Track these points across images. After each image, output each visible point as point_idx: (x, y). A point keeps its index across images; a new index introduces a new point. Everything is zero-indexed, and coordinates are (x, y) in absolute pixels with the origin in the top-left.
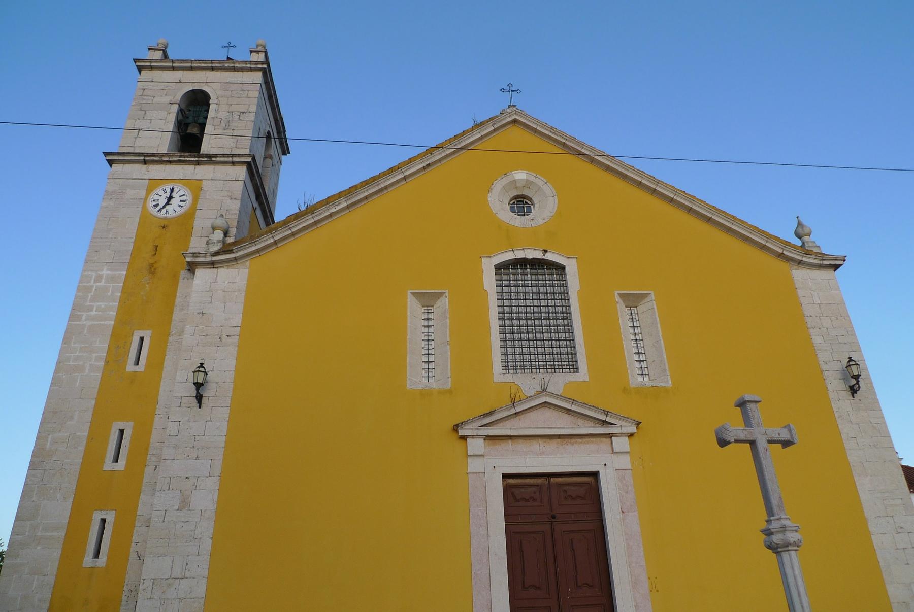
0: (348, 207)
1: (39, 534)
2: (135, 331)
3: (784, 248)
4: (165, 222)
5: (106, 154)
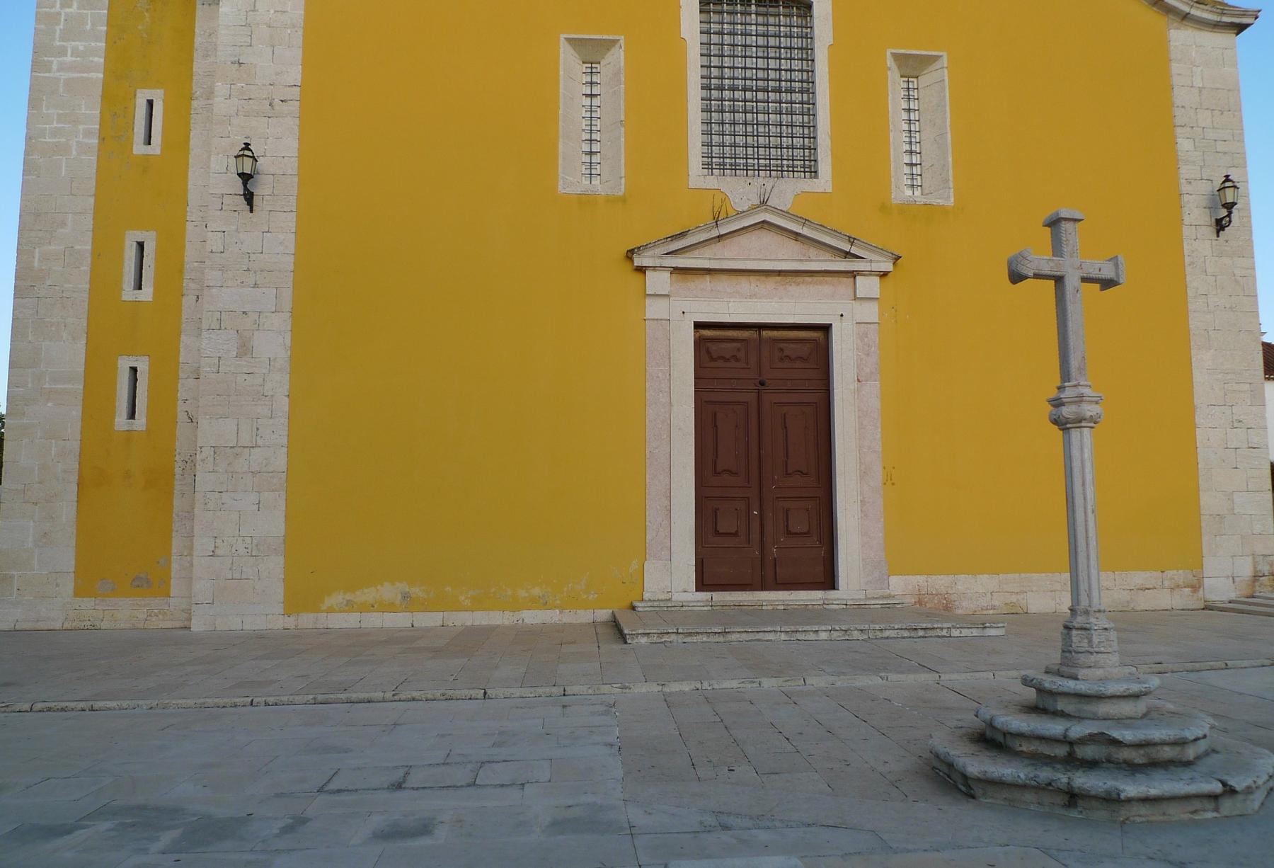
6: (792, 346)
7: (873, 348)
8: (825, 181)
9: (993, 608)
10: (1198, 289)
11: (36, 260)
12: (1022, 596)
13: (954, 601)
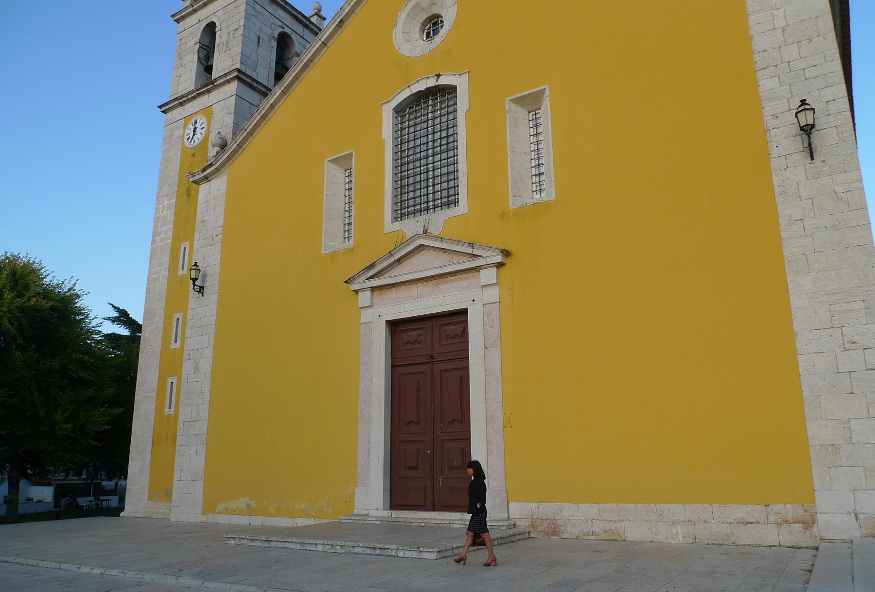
0: (284, 93)
1: (146, 395)
2: (182, 244)
4: (193, 151)
5: (160, 107)
6: (453, 327)
7: (496, 321)
8: (462, 207)
9: (594, 534)
10: (791, 216)
11: (147, 334)
12: (620, 525)
13: (560, 526)
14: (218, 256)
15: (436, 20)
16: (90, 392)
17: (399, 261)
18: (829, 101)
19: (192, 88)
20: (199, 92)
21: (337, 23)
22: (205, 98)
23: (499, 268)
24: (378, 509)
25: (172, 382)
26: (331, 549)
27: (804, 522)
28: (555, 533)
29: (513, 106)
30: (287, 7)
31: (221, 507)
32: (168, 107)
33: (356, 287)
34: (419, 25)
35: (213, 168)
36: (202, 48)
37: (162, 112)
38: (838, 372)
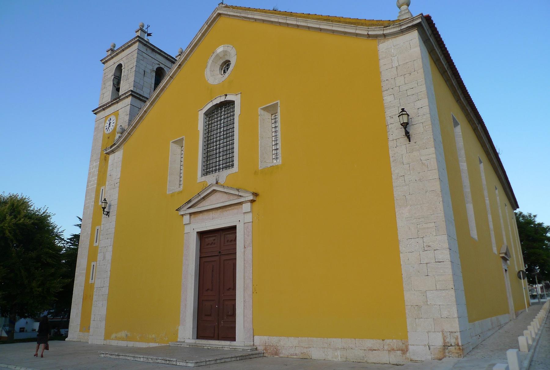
3: (367, 29)
5: (93, 111)
8: (235, 169)
9: (296, 355)
12: (309, 349)
13: (279, 350)
14: (117, 195)
15: (228, 63)
16: (53, 270)
17: (204, 198)
18: (419, 108)
19: (110, 100)
20: (112, 103)
21: (177, 66)
22: (115, 106)
23: (252, 203)
24: (189, 339)
25: (94, 265)
26: (146, 360)
27: (402, 350)
28: (276, 354)
29: (262, 112)
30: (162, 53)
31: (113, 336)
32: (97, 111)
33: (182, 213)
34: (219, 66)
35: (116, 146)
36: (116, 78)
37: (94, 114)
38: (421, 264)
